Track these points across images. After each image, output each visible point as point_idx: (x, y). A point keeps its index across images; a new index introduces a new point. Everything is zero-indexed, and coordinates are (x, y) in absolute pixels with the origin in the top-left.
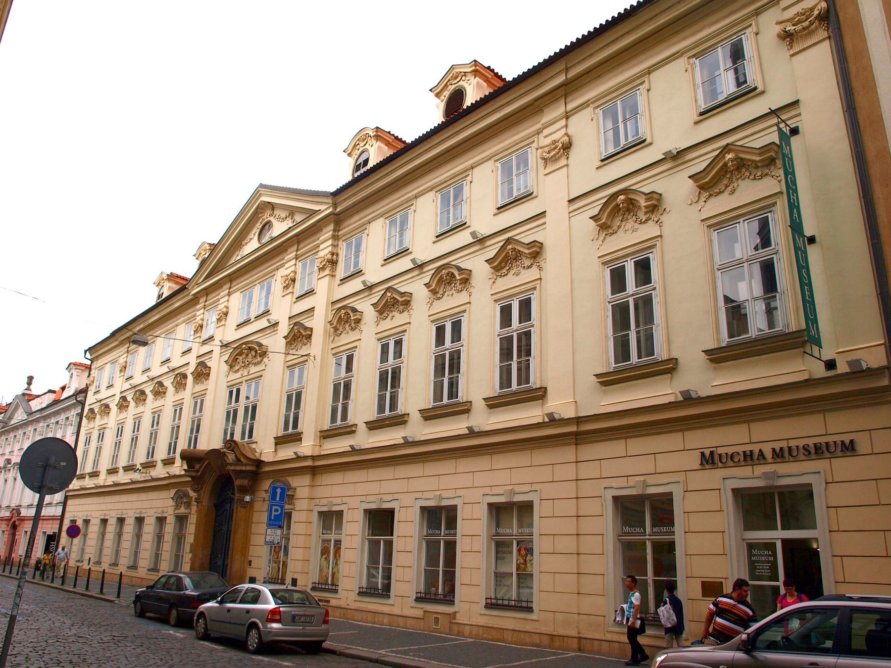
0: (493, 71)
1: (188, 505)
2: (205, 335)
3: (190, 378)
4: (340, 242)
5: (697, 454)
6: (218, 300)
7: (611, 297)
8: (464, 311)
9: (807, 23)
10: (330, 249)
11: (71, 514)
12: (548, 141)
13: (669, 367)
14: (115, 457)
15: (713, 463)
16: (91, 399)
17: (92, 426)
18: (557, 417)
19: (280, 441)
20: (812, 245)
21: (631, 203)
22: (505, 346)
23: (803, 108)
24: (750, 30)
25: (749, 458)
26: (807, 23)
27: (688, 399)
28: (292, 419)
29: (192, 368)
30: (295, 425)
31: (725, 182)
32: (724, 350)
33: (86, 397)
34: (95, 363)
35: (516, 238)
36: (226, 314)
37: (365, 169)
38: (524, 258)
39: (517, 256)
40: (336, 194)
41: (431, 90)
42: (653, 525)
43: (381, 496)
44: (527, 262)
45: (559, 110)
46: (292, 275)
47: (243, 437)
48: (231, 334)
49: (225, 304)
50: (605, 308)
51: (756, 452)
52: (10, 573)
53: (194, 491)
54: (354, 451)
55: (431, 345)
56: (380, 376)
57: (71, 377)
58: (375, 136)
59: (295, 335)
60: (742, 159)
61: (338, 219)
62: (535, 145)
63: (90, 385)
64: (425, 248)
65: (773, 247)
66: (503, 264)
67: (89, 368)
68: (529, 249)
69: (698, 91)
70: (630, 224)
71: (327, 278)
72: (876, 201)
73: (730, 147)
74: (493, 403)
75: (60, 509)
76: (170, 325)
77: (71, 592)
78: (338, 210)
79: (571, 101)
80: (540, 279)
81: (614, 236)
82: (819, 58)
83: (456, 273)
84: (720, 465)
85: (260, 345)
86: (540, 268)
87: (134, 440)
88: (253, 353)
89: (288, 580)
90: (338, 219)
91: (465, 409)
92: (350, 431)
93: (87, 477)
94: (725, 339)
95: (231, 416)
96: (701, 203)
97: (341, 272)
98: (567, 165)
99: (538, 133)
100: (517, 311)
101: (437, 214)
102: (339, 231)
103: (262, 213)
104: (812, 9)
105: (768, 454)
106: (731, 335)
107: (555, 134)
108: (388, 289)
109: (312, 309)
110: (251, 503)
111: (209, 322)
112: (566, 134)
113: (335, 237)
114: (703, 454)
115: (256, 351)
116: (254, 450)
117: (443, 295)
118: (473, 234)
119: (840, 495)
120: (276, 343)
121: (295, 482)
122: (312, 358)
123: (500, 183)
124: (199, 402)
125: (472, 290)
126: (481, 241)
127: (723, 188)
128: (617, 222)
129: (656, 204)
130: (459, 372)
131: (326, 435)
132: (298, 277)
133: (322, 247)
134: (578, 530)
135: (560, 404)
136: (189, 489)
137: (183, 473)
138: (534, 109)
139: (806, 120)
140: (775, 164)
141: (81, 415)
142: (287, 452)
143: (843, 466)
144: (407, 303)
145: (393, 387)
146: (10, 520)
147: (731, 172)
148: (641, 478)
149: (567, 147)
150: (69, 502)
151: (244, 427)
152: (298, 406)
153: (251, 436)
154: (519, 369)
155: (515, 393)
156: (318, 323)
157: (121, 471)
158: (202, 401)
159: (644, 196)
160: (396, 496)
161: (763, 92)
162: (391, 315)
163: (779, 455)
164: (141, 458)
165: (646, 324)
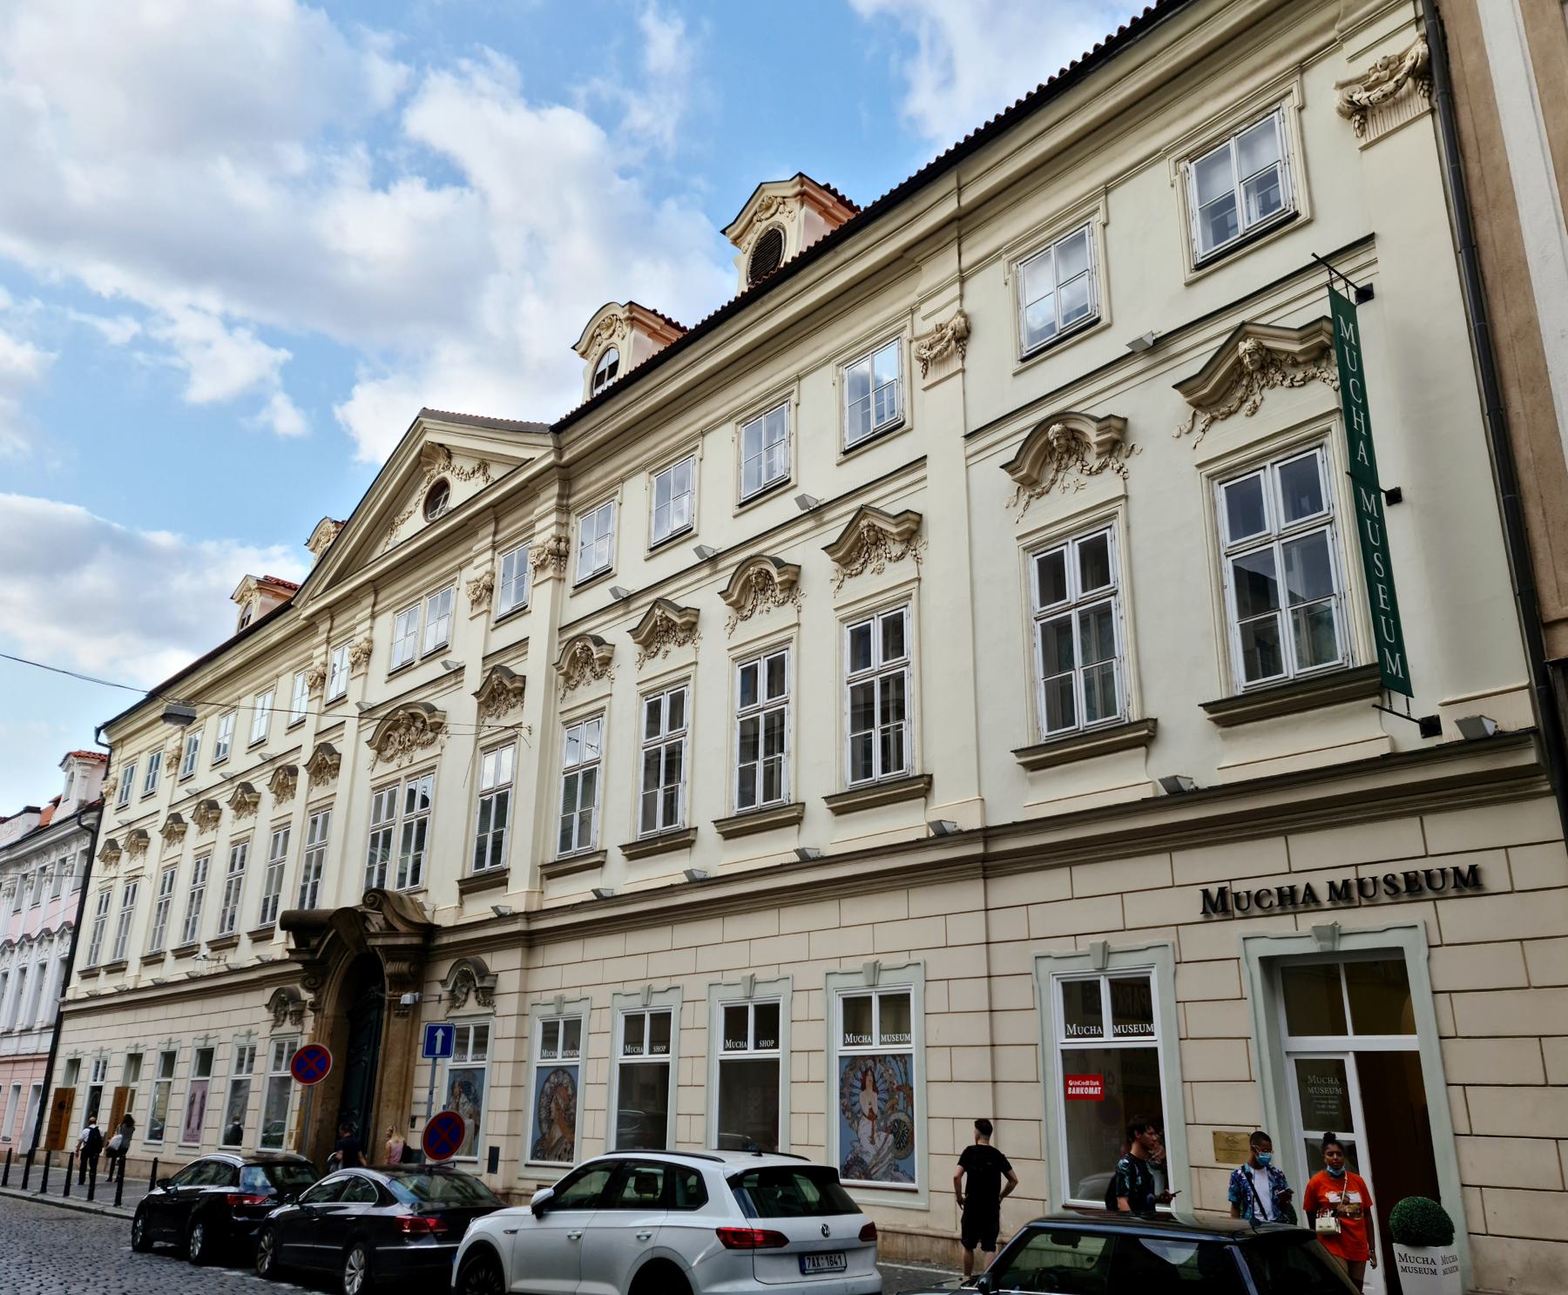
0: (834, 192)
1: (299, 1017)
2: (332, 693)
3: (303, 776)
4: (573, 515)
6: (353, 628)
7: (1039, 609)
8: (789, 640)
9: (1391, 84)
10: (553, 530)
11: (71, 1049)
12: (929, 326)
13: (1145, 735)
14: (158, 933)
15: (1225, 910)
18: (949, 828)
19: (468, 887)
20: (1395, 507)
21: (1074, 439)
22: (861, 700)
24: (1288, 100)
25: (1290, 901)
26: (1391, 84)
27: (1177, 793)
28: (490, 847)
29: (306, 755)
30: (496, 858)
31: (1239, 394)
32: (1236, 703)
33: (99, 818)
34: (118, 752)
35: (876, 505)
36: (369, 653)
37: (615, 379)
38: (890, 543)
39: (879, 538)
40: (559, 428)
41: (723, 232)
43: (649, 982)
44: (896, 549)
45: (943, 267)
46: (487, 578)
47: (401, 884)
48: (379, 691)
49: (367, 634)
50: (1031, 631)
51: (1301, 888)
53: (309, 989)
54: (601, 899)
55: (733, 704)
56: (647, 761)
57: (71, 781)
58: (628, 319)
59: (493, 690)
60: (1269, 350)
61: (566, 474)
62: (906, 334)
63: (108, 794)
64: (722, 529)
65: (1325, 511)
66: (854, 554)
67: (106, 761)
68: (897, 525)
69: (1193, 225)
70: (1073, 474)
71: (550, 583)
73: (1249, 328)
74: (842, 805)
75: (47, 1039)
76: (263, 674)
77: (62, 1206)
78: (566, 457)
79: (970, 248)
81: (1045, 498)
82: (1415, 144)
83: (773, 571)
84: (1237, 913)
85: (431, 709)
86: (918, 559)
87: (196, 897)
88: (419, 725)
90: (566, 474)
91: (794, 817)
92: (595, 862)
93: (103, 973)
94: (1240, 683)
95: (381, 841)
97: (577, 570)
98: (963, 371)
99: (912, 312)
100: (881, 637)
101: (739, 465)
102: (569, 497)
103: (429, 464)
104: (1401, 58)
105: (1323, 894)
106: (1250, 677)
108: (656, 603)
109: (524, 642)
110: (416, 1006)
111: (337, 669)
112: (961, 312)
113: (563, 509)
114: (1206, 893)
115: (424, 722)
116: (420, 908)
117: (752, 611)
119: (1453, 969)
120: (459, 706)
121: (495, 962)
123: (847, 405)
124: (319, 818)
125: (801, 600)
126: (816, 512)
127: (1236, 404)
129: (1118, 439)
130: (782, 750)
131: (551, 872)
132: (498, 583)
134: (992, 1037)
135: (954, 805)
136: (298, 986)
137: (287, 956)
138: (904, 264)
139: (1383, 271)
140: (1329, 358)
141: (90, 854)
142: (480, 907)
143: (1458, 915)
144: (691, 628)
145: (669, 780)
147: (1250, 375)
148: (1100, 939)
149: (962, 337)
150: (67, 1025)
151: (403, 862)
153: (415, 880)
154: (885, 741)
155: (879, 786)
156: (535, 667)
157: (170, 958)
158: (326, 818)
159: (1094, 425)
160: (676, 982)
161: (1309, 222)
162: (663, 649)
163: (1342, 895)
164: (208, 930)
165: (1102, 658)
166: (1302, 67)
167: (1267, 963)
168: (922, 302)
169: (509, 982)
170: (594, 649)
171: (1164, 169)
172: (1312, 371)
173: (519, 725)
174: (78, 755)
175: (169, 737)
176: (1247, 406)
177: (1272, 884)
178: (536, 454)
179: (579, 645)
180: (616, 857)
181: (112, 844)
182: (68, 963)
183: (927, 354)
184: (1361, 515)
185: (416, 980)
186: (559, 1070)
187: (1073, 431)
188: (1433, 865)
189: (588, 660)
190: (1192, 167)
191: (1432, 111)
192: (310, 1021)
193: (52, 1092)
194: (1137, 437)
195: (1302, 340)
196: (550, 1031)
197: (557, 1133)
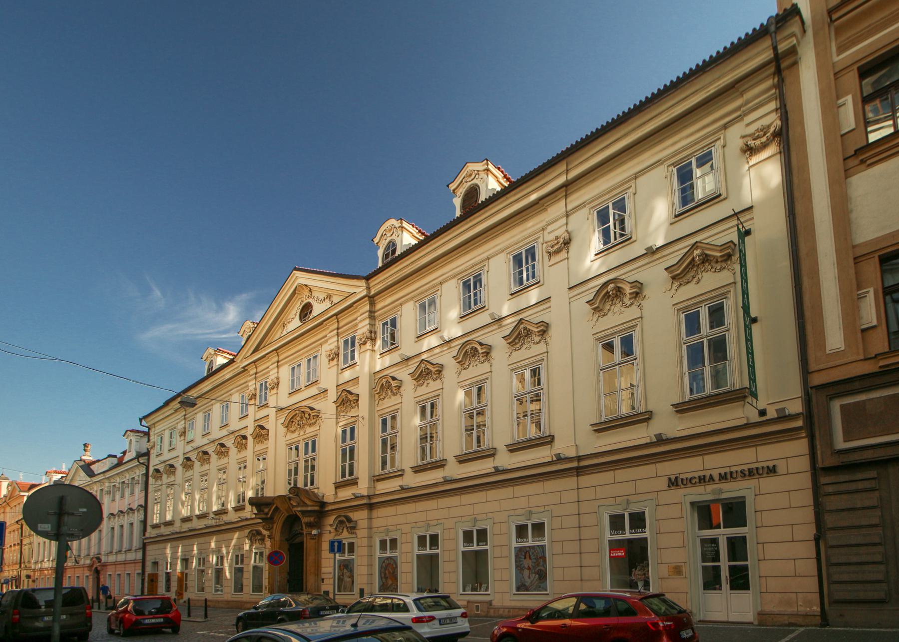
3: (250, 440)
5: (666, 479)
12: (551, 237)
16: (154, 461)
17: (160, 483)
18: (562, 456)
19: (338, 486)
23: (755, 213)
24: (719, 142)
25: (702, 480)
27: (661, 440)
30: (351, 474)
33: (149, 460)
34: (153, 430)
39: (528, 333)
42: (631, 528)
44: (537, 339)
45: (558, 209)
52: (99, 608)
53: (266, 530)
60: (707, 255)
62: (540, 240)
67: (147, 434)
70: (618, 307)
72: (804, 287)
78: (372, 293)
79: (571, 202)
80: (642, 318)
83: (479, 347)
88: (307, 415)
89: (356, 590)
94: (688, 397)
96: (673, 291)
99: (543, 230)
104: (769, 126)
105: (716, 477)
107: (558, 230)
110: (320, 535)
114: (670, 479)
117: (469, 365)
118: (492, 315)
122: (360, 419)
128: (607, 306)
133: (360, 326)
135: (564, 446)
136: (261, 529)
142: (346, 494)
143: (767, 483)
146: (92, 566)
149: (567, 243)
150: (149, 548)
151: (306, 477)
152: (352, 458)
159: (629, 285)
161: (725, 199)
163: (723, 477)
166: (725, 127)
167: (693, 504)
168: (548, 225)
169: (363, 524)
170: (392, 382)
171: (661, 170)
172: (724, 265)
173: (358, 416)
174: (132, 431)
175: (177, 421)
176: (695, 279)
177: (696, 475)
178: (357, 290)
179: (384, 380)
180: (409, 472)
181: (157, 471)
182: (144, 522)
183: (551, 250)
184: (746, 326)
185: (318, 524)
186: (388, 558)
187: (619, 288)
188: (759, 465)
189: (389, 386)
190: (675, 170)
191: (780, 153)
192: (268, 543)
193: (146, 575)
194: (646, 292)
195: (721, 251)
196: (383, 543)
197: (390, 582)
